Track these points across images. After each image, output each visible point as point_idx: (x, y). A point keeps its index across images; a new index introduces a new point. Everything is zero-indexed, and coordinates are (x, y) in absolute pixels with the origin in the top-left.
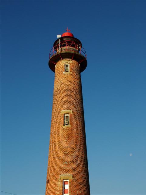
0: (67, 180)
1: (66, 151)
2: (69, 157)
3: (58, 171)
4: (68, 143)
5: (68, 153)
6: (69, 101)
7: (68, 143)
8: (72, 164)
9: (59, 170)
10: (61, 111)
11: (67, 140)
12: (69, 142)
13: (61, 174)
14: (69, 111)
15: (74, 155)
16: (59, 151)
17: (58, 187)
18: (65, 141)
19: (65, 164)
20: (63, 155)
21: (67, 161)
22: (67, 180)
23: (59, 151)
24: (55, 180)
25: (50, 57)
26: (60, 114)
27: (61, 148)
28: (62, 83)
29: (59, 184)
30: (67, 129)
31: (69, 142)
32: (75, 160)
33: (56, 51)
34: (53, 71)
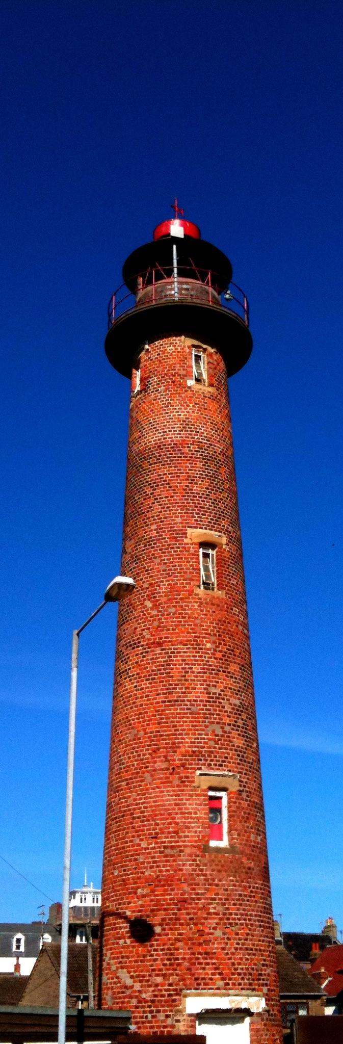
0: (219, 794)
1: (215, 686)
2: (224, 707)
3: (190, 756)
4: (218, 655)
5: (220, 694)
6: (212, 496)
7: (218, 655)
8: (234, 733)
9: (194, 752)
10: (189, 531)
11: (214, 642)
12: (220, 651)
13: (200, 769)
14: (214, 535)
15: (237, 702)
16: (187, 680)
17: (190, 813)
18: (208, 645)
19: (213, 731)
20: (204, 697)
21: (218, 723)
22: (219, 794)
23: (187, 680)
24: (178, 786)
25: (110, 320)
26: (186, 541)
27: (197, 669)
28: (186, 424)
29: (196, 806)
30: (213, 604)
31: (220, 651)
32: (240, 723)
33: (134, 289)
34: (127, 377)
